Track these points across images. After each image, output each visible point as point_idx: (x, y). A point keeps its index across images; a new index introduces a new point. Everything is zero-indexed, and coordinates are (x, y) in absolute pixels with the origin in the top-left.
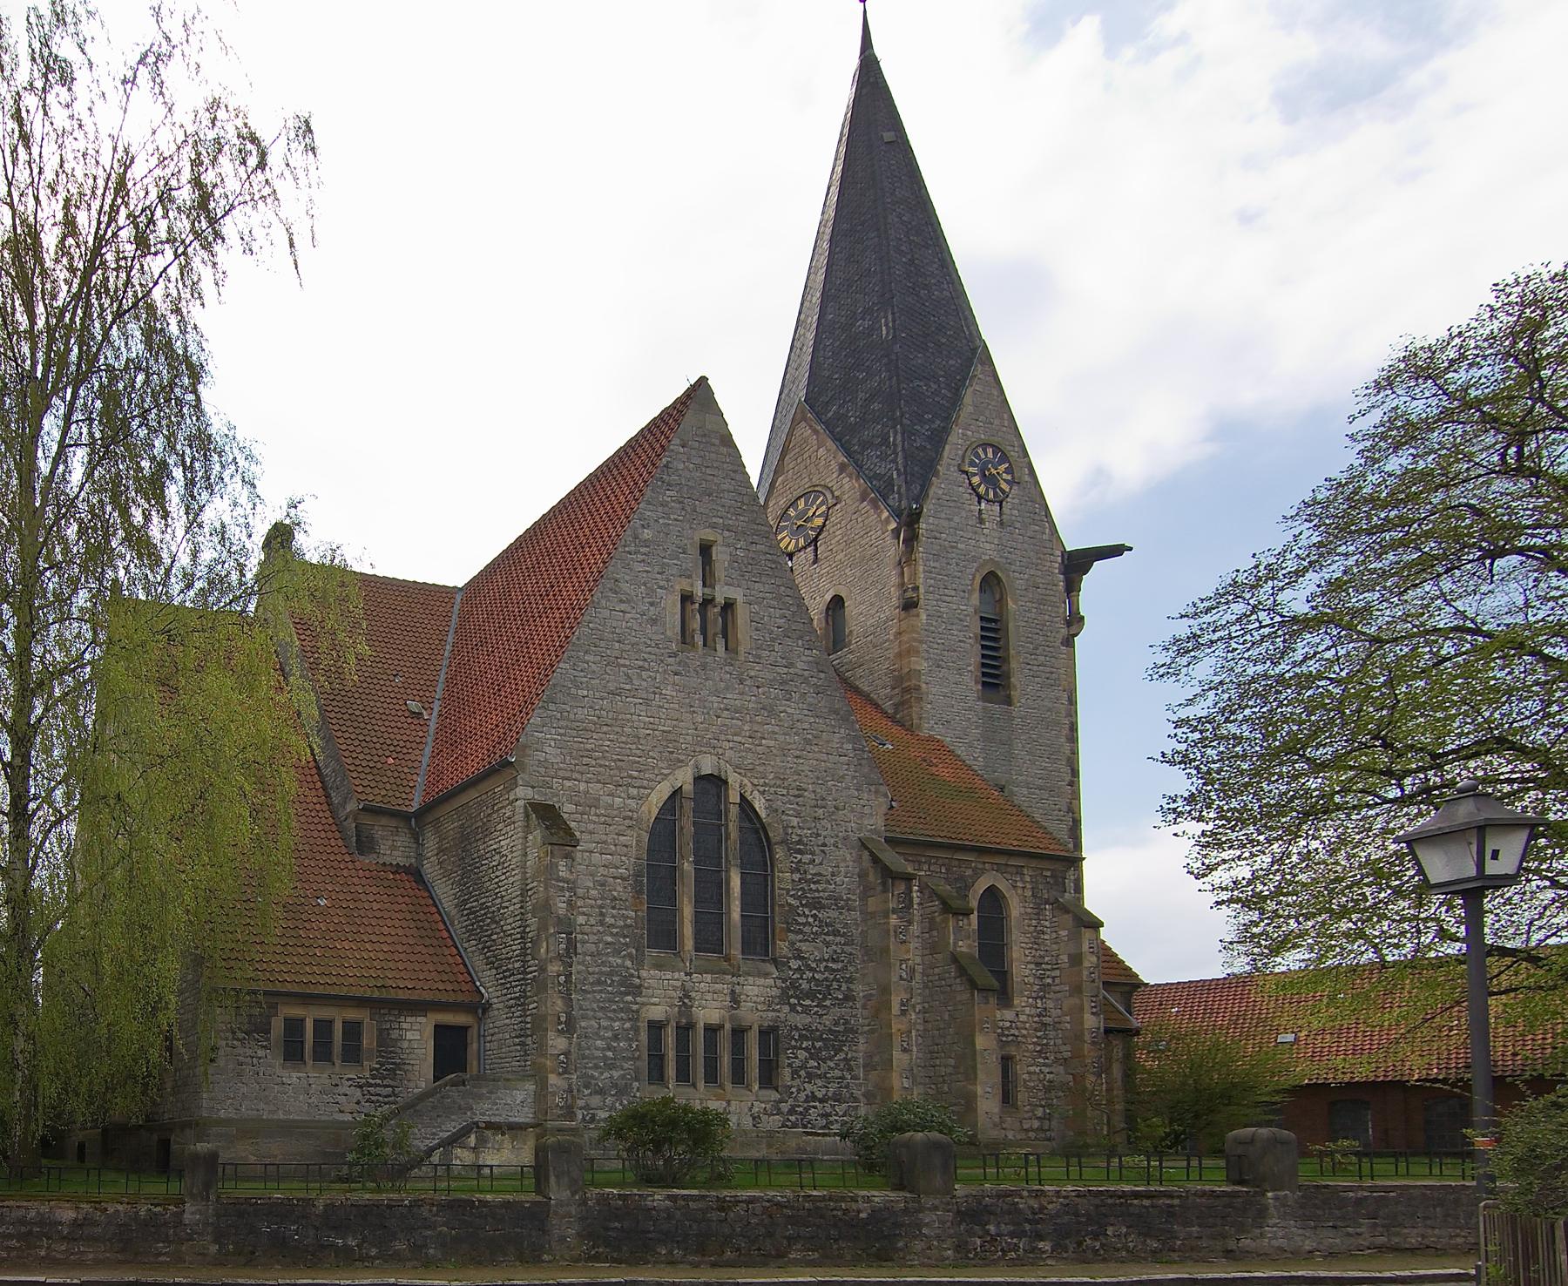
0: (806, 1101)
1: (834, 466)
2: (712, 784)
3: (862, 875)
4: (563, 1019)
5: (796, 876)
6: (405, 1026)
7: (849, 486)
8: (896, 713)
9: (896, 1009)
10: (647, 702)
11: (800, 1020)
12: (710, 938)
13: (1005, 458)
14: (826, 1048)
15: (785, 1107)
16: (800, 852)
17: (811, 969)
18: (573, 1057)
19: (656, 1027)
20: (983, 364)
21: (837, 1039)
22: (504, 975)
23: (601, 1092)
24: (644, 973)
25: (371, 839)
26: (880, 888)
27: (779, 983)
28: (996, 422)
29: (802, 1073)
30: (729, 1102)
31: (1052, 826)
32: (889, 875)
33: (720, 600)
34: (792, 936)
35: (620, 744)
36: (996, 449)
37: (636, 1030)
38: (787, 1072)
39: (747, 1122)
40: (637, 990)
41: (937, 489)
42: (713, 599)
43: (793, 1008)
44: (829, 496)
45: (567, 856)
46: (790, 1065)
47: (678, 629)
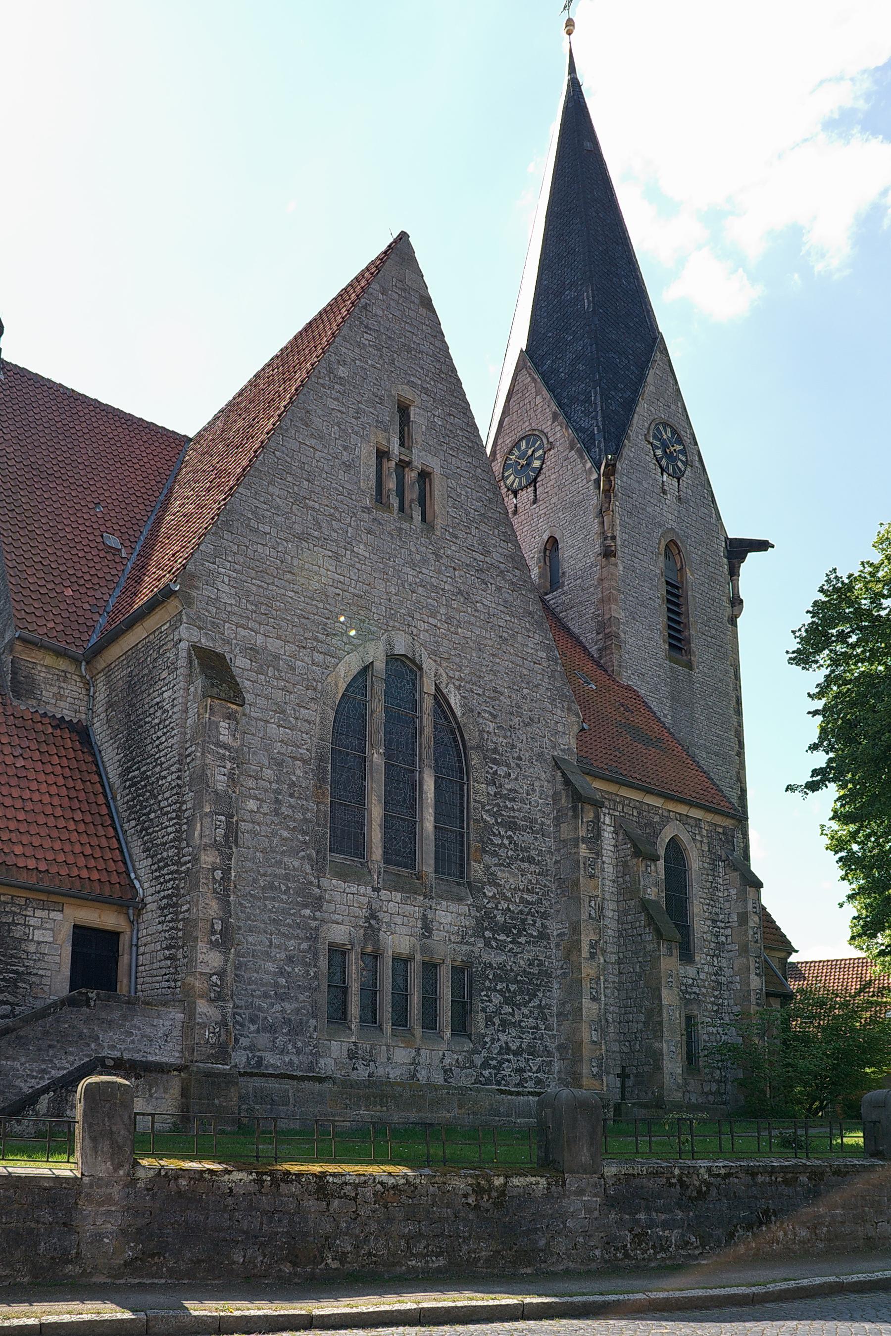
0: (499, 1053)
1: (549, 415)
2: (403, 668)
3: (556, 797)
4: (218, 927)
5: (492, 790)
6: (32, 921)
7: (559, 434)
8: (600, 658)
9: (585, 954)
10: (337, 557)
11: (495, 958)
12: (401, 850)
13: (680, 441)
14: (521, 992)
15: (478, 1060)
16: (495, 761)
17: (506, 899)
18: (230, 978)
19: (338, 953)
20: (661, 352)
21: (532, 983)
22: (160, 864)
23: (271, 1029)
24: (325, 883)
25: (30, 677)
26: (571, 814)
27: (474, 913)
28: (673, 407)
29: (497, 1021)
30: (418, 1050)
31: (727, 791)
32: (578, 798)
33: (417, 464)
34: (486, 857)
35: (318, 614)
36: (674, 432)
37: (316, 955)
38: (480, 1017)
39: (438, 1078)
40: (317, 903)
41: (628, 451)
42: (409, 463)
43: (487, 944)
44: (545, 441)
45: (231, 716)
46: (484, 1010)
47: (373, 483)
